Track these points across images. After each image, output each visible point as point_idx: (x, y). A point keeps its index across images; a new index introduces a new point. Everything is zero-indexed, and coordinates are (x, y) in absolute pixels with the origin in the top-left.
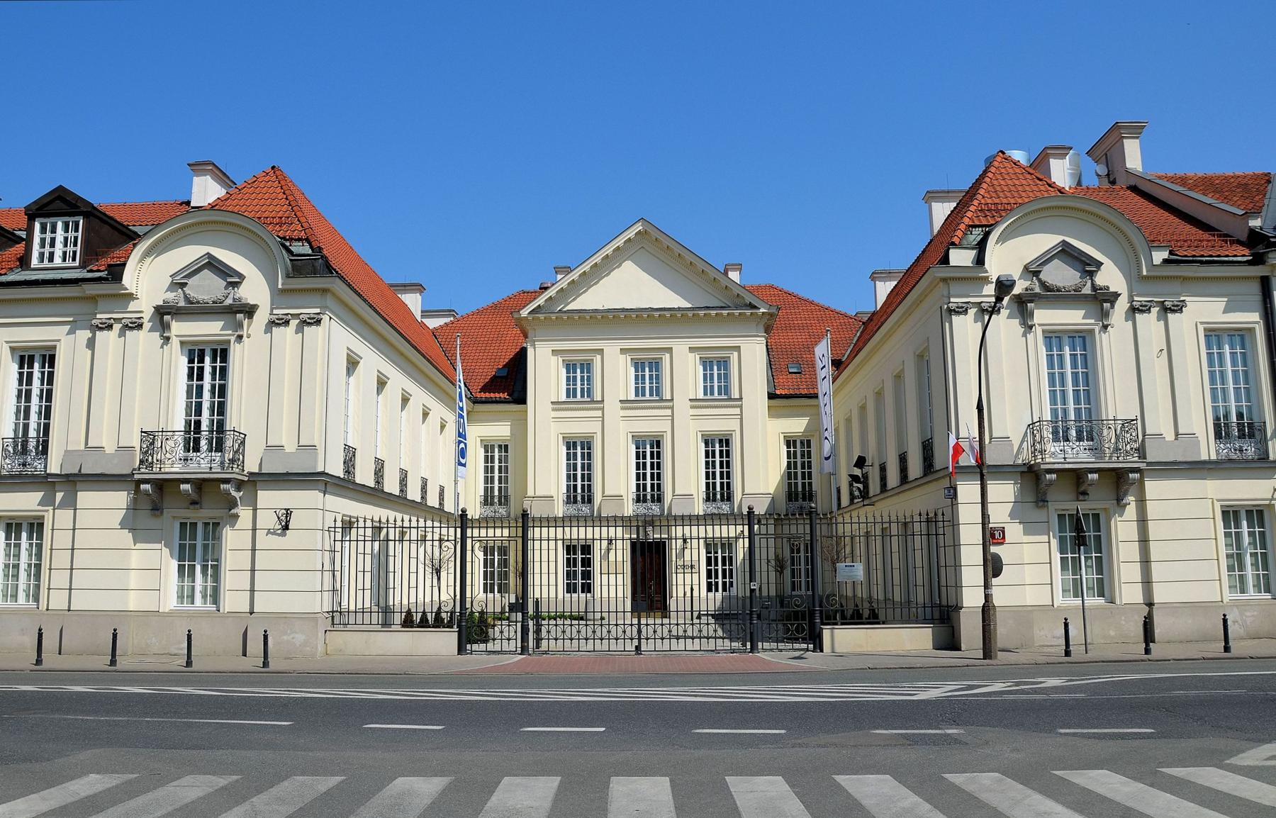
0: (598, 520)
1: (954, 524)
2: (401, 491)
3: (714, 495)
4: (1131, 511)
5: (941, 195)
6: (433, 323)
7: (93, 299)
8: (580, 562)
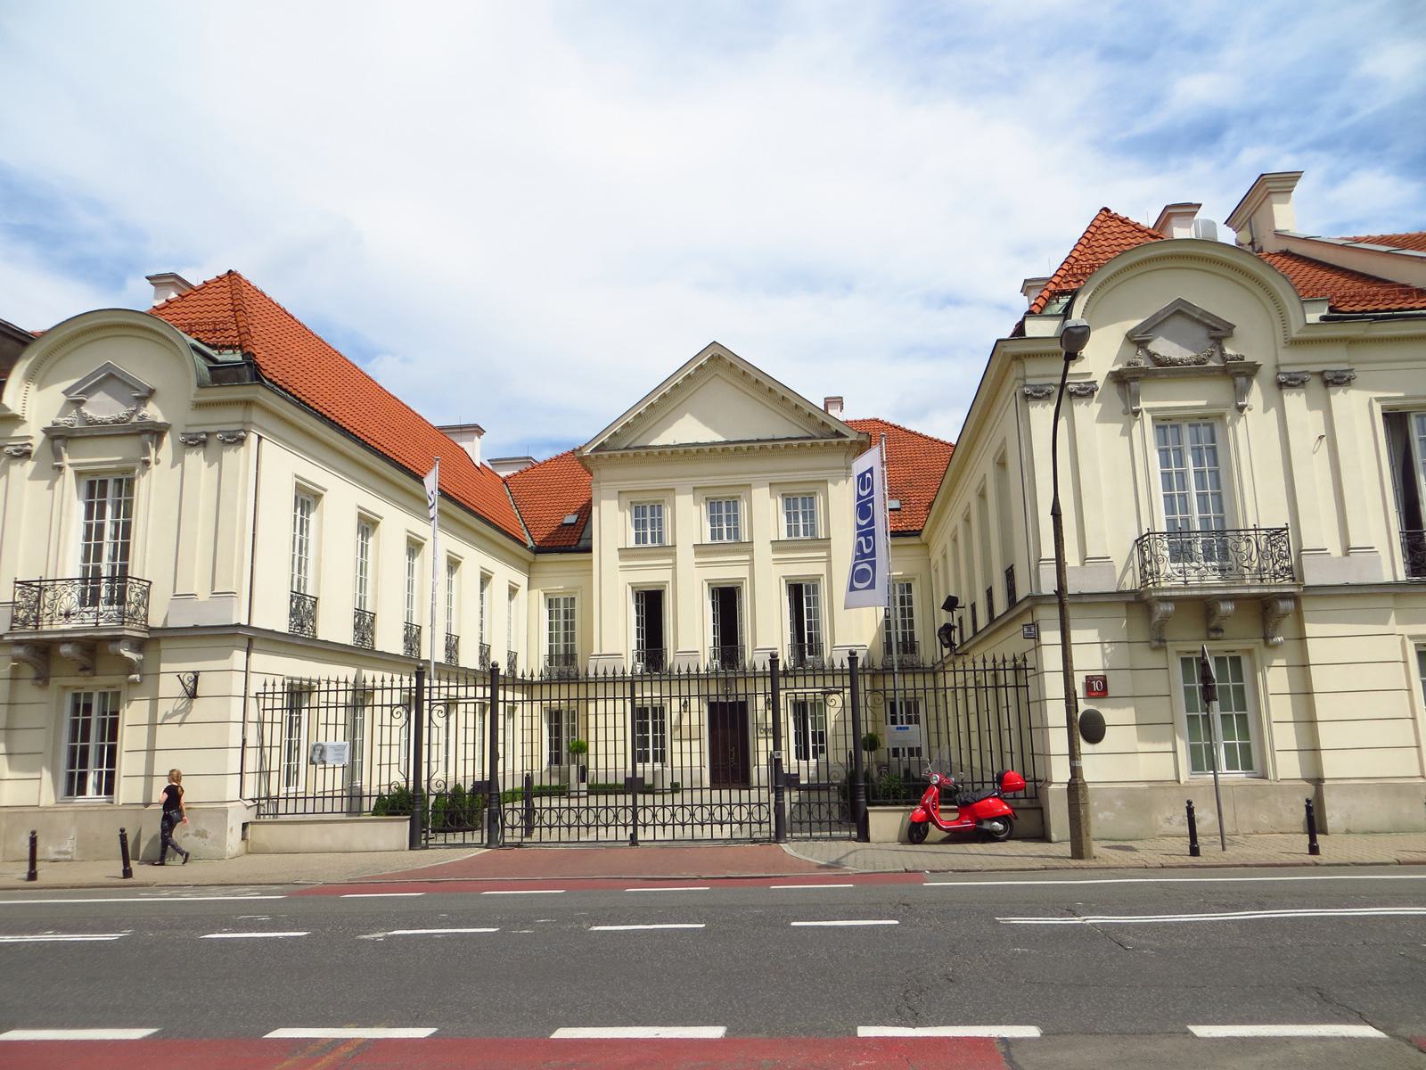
1: (1039, 673)
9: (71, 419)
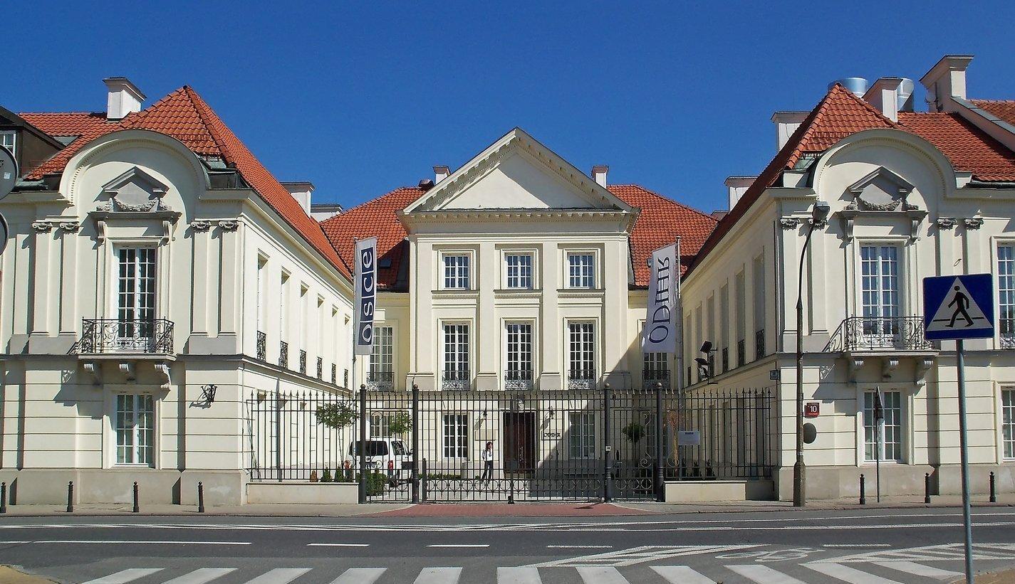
0: (470, 393)
1: (778, 400)
2: (259, 354)
3: (579, 373)
4: (923, 392)
5: (787, 118)
6: (321, 217)
7: (33, 206)
8: (457, 425)
9: (107, 206)
